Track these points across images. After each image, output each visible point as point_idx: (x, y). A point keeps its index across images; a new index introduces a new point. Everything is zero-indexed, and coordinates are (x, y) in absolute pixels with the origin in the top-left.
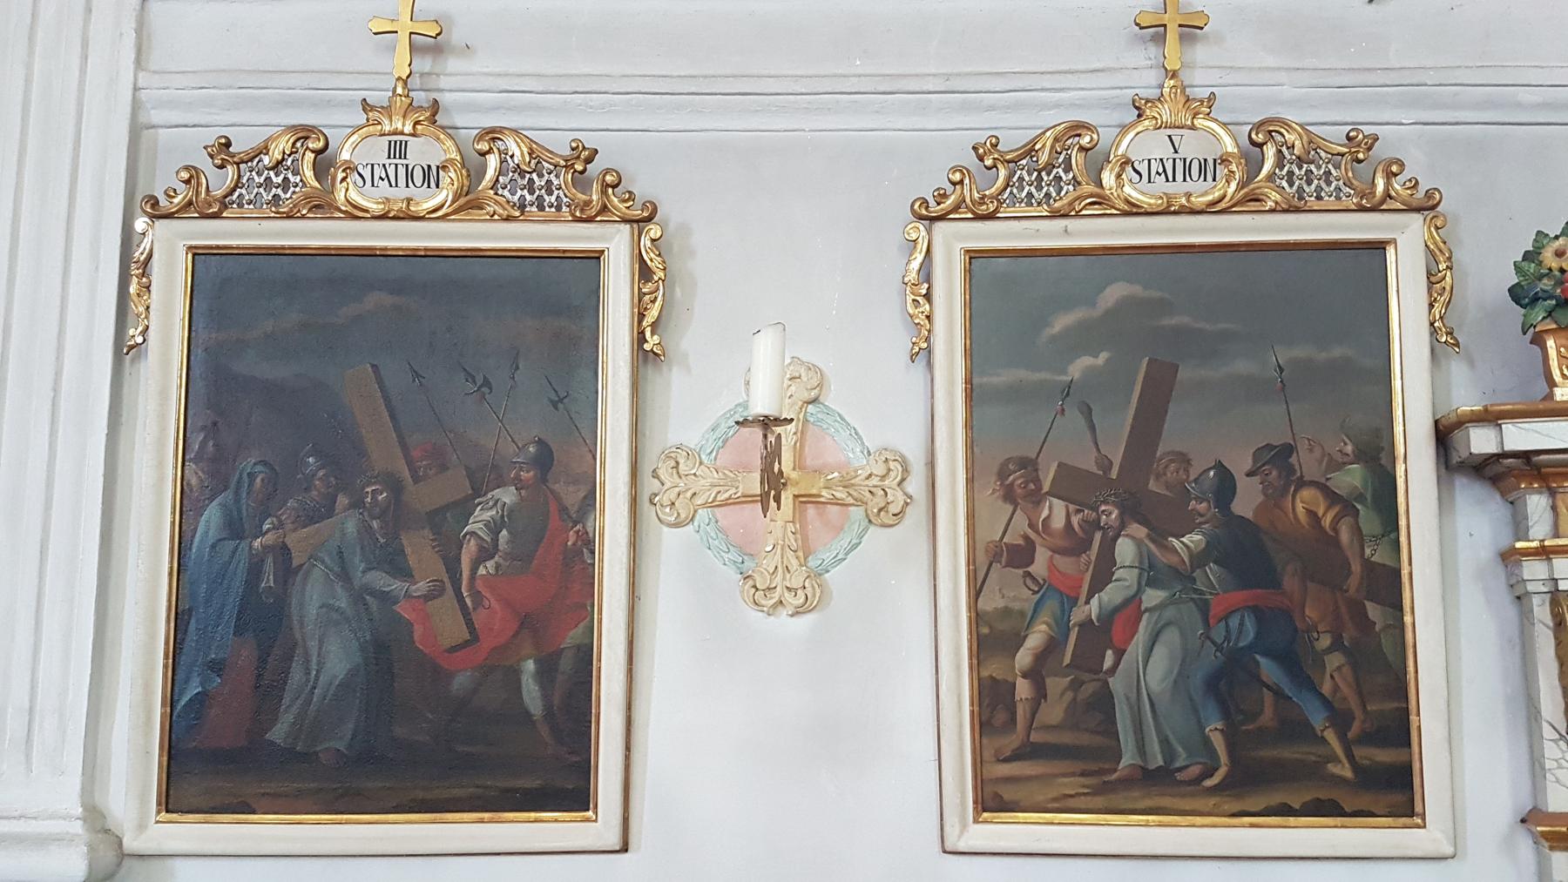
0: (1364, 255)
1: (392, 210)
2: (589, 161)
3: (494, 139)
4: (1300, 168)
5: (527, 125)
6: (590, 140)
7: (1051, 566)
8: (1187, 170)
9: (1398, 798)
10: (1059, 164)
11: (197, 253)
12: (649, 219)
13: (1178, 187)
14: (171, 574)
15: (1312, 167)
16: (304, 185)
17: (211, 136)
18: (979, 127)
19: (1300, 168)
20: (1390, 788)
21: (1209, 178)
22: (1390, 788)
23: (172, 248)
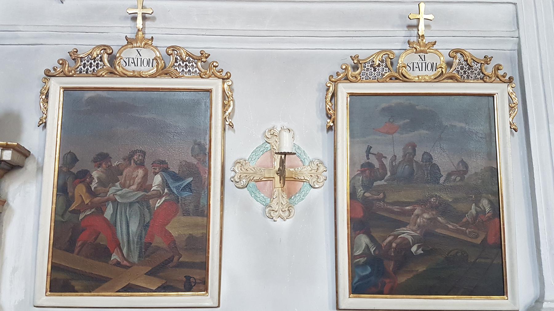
0: (485, 99)
1: (138, 75)
2: (206, 58)
3: (174, 50)
4: (183, 63)
5: (189, 46)
6: (207, 51)
7: (86, 200)
8: (427, 67)
9: (202, 287)
10: (109, 60)
11: (66, 89)
12: (228, 78)
13: (424, 73)
14: (503, 208)
15: (187, 63)
16: (104, 65)
17: (71, 49)
18: (69, 44)
19: (183, 63)
20: (499, 289)
21: (151, 65)
22: (499, 289)
23: (56, 87)
